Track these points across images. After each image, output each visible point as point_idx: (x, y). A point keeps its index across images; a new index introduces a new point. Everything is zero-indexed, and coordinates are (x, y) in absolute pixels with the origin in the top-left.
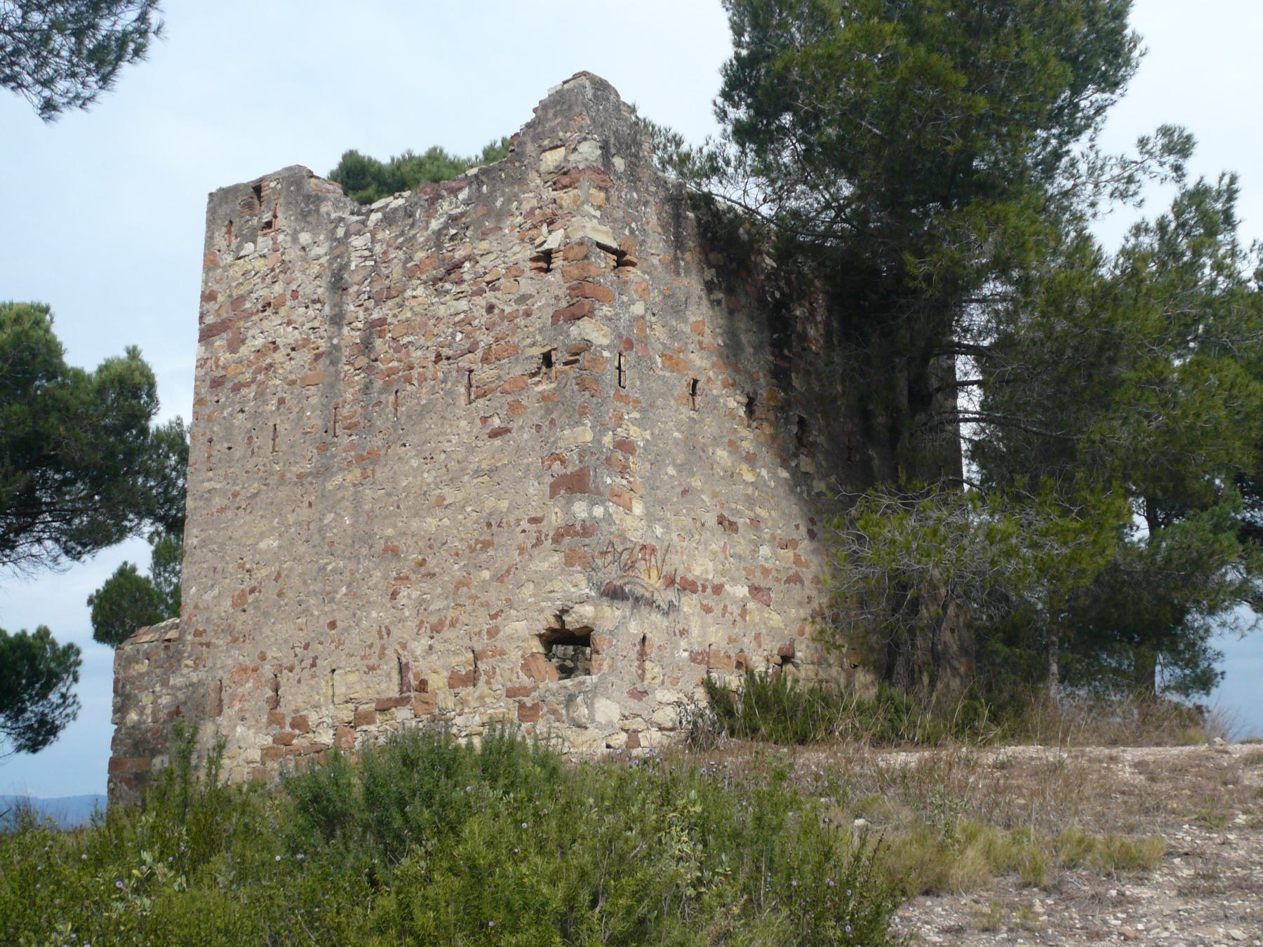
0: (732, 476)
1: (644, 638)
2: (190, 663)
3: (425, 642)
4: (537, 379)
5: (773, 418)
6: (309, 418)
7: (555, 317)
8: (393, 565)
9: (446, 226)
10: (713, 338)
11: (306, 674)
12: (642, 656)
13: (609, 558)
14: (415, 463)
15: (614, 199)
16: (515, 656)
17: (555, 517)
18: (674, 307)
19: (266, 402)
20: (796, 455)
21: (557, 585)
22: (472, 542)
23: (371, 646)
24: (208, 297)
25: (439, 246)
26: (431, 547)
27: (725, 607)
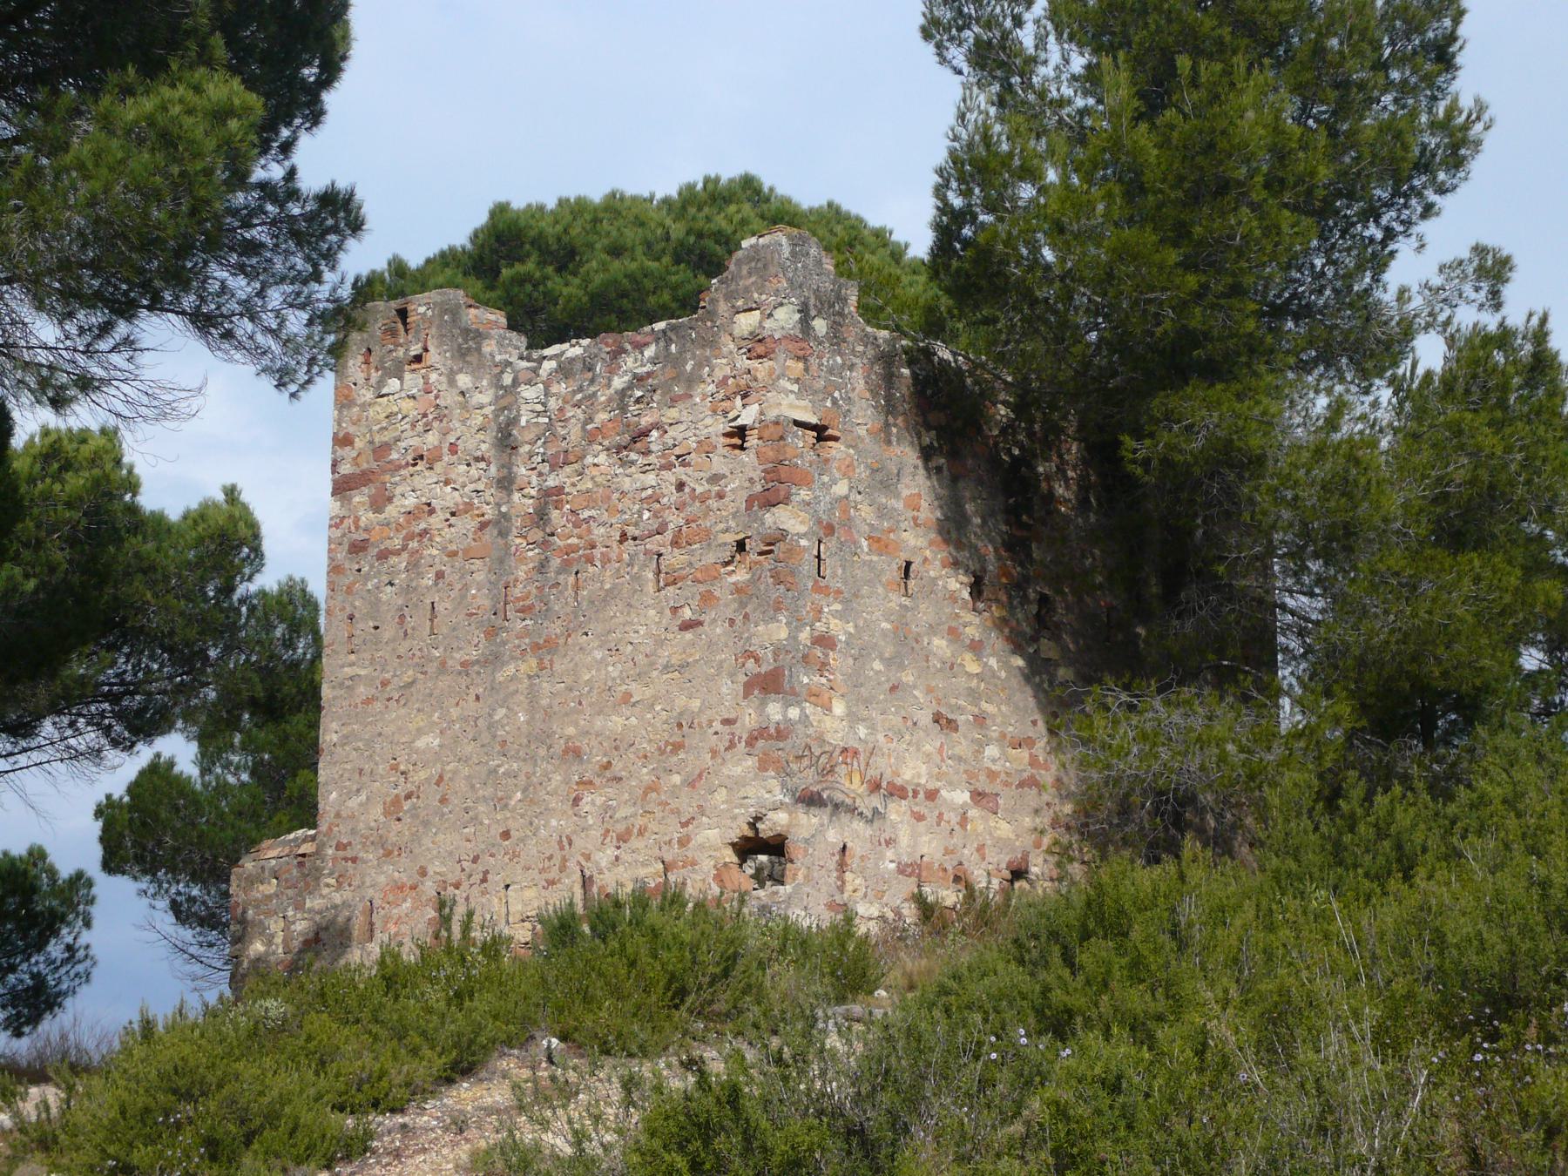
0: (952, 667)
1: (844, 847)
2: (332, 881)
3: (611, 852)
4: (730, 568)
5: (1004, 598)
6: (474, 597)
7: (750, 501)
8: (574, 768)
9: (630, 387)
10: (929, 512)
11: (475, 891)
12: (842, 867)
13: (806, 762)
14: (598, 655)
15: (814, 367)
16: (707, 865)
17: (749, 719)
18: (884, 481)
19: (421, 575)
20: (1035, 639)
21: (750, 791)
22: (662, 744)
23: (550, 858)
24: (342, 441)
25: (623, 409)
26: (616, 748)
27: (941, 815)
